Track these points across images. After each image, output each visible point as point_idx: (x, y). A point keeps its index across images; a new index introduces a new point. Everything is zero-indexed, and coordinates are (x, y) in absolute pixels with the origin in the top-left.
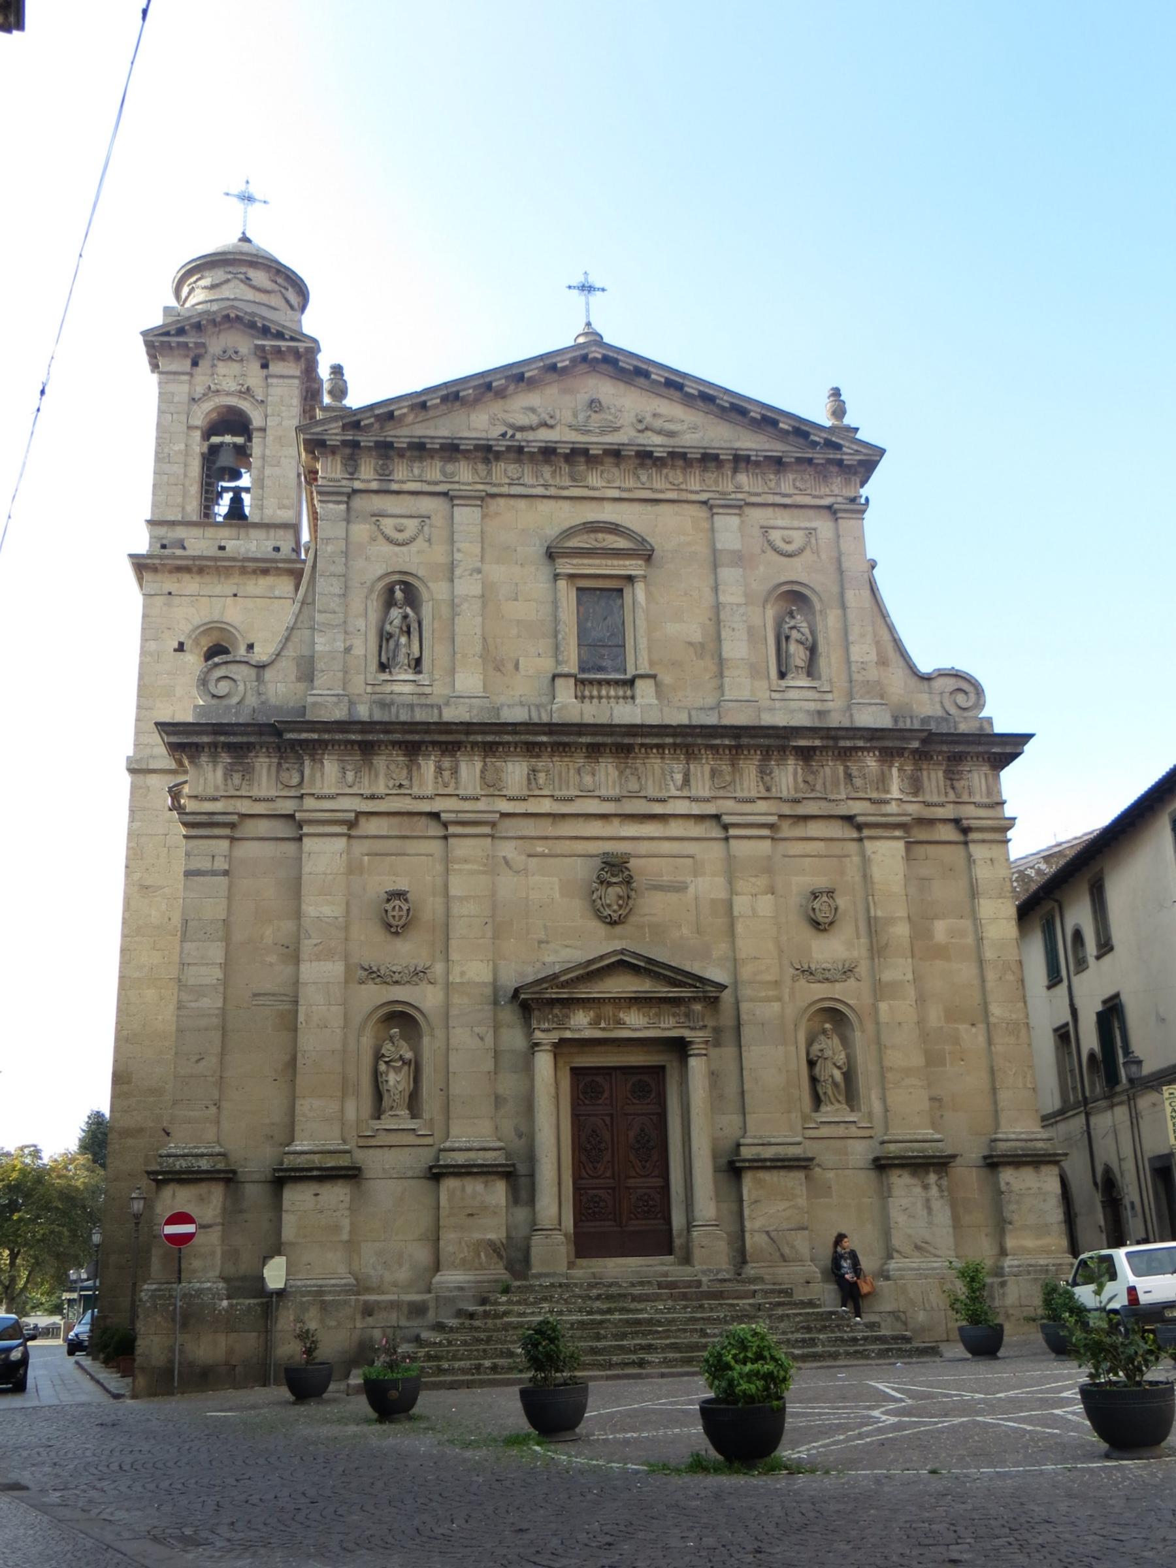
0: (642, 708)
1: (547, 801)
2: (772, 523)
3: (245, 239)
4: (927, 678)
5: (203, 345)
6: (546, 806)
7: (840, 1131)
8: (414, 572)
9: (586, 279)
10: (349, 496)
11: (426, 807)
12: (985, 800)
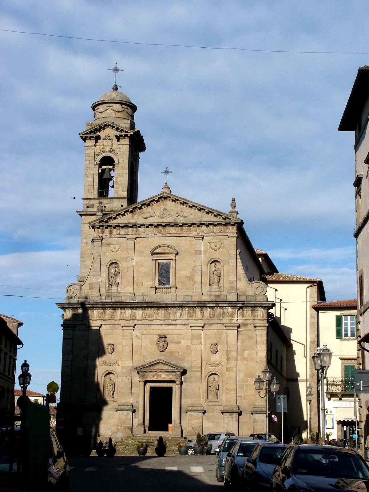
8: (118, 259)
9: (167, 169)
12: (262, 319)
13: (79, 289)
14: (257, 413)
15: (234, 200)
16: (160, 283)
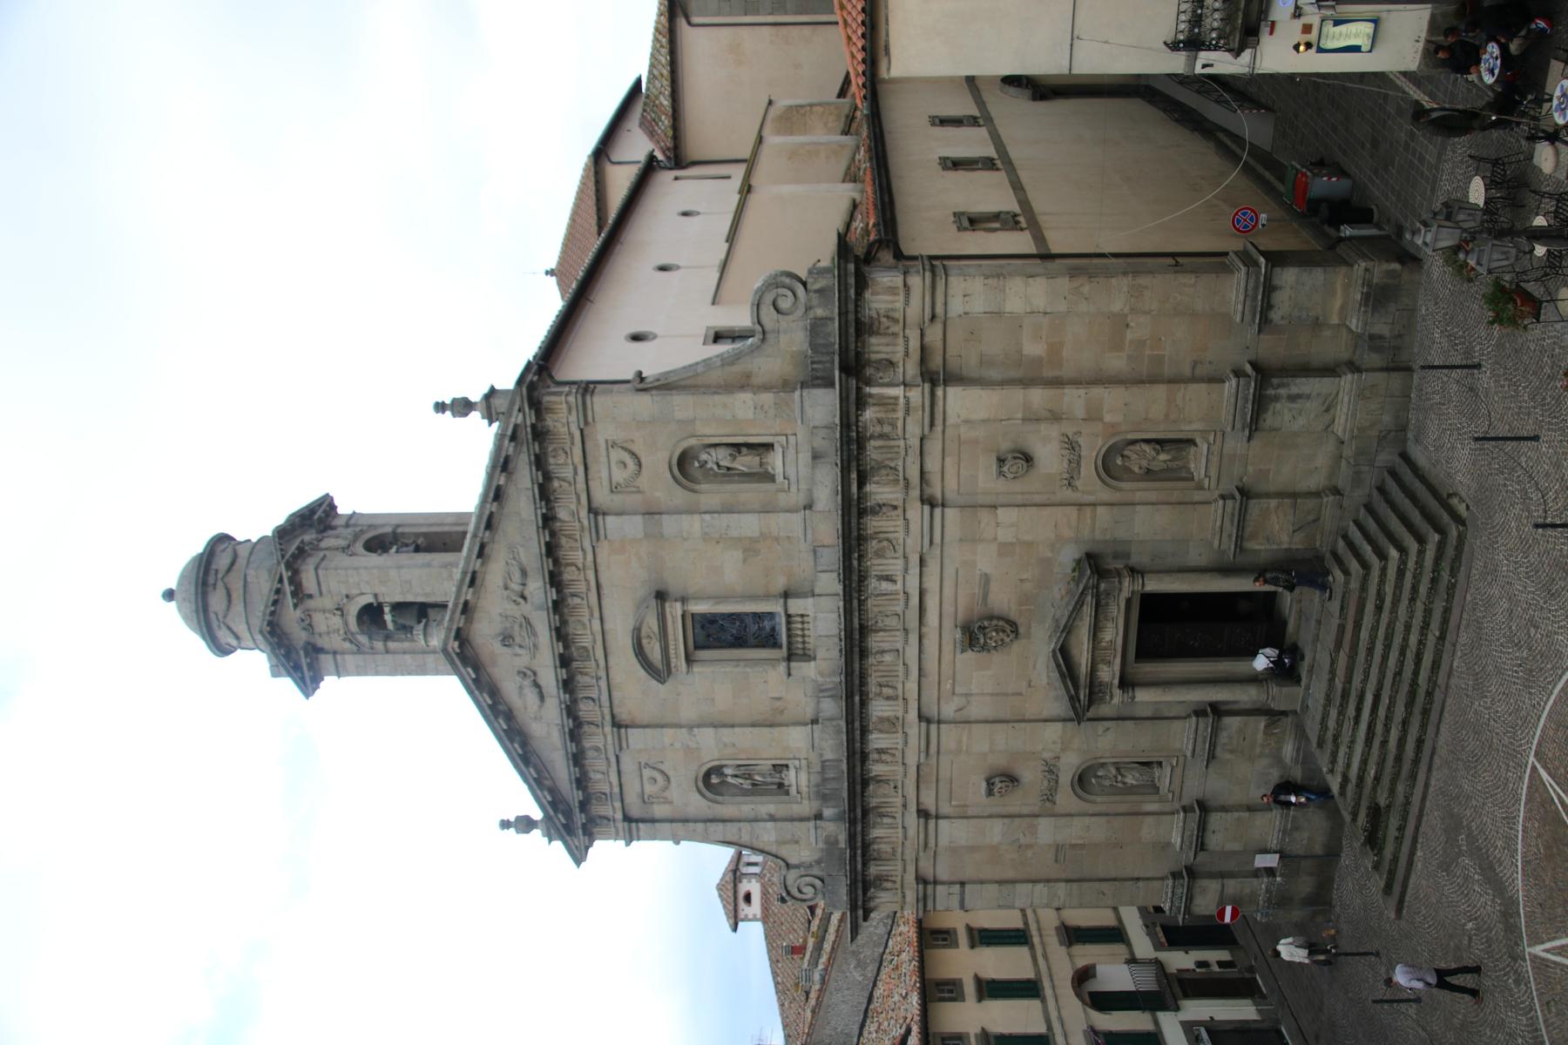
1: (908, 685)
2: (606, 483)
7: (1215, 459)
12: (901, 298)
14: (1267, 306)
15: (440, 407)
16: (770, 641)
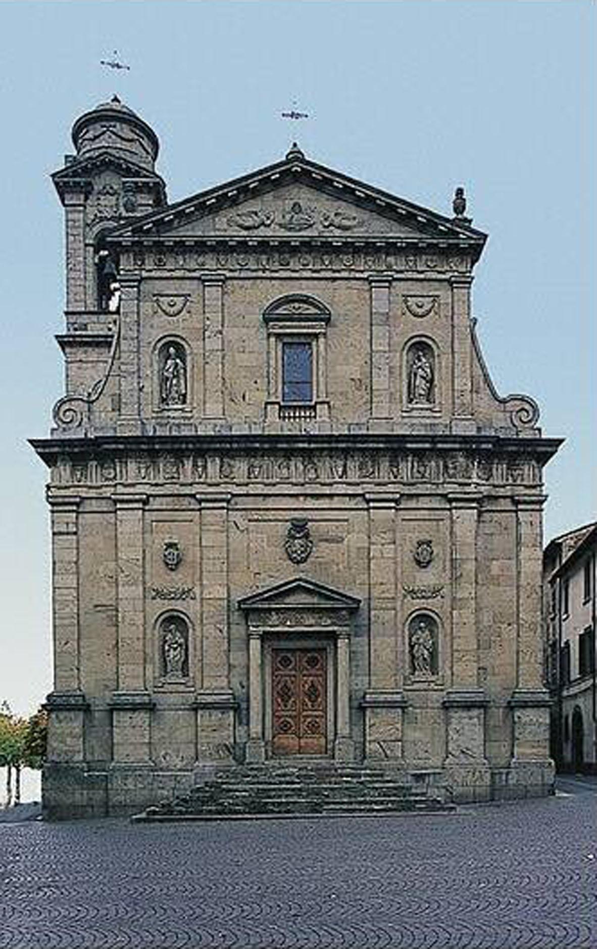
0: (320, 424)
3: (116, 99)
4: (503, 402)
5: (90, 184)
6: (260, 489)
10: (140, 281)
11: (187, 490)
13: (86, 409)
15: (460, 192)
